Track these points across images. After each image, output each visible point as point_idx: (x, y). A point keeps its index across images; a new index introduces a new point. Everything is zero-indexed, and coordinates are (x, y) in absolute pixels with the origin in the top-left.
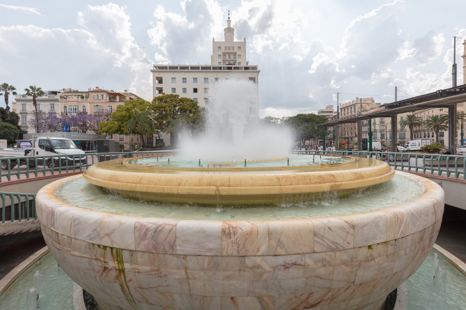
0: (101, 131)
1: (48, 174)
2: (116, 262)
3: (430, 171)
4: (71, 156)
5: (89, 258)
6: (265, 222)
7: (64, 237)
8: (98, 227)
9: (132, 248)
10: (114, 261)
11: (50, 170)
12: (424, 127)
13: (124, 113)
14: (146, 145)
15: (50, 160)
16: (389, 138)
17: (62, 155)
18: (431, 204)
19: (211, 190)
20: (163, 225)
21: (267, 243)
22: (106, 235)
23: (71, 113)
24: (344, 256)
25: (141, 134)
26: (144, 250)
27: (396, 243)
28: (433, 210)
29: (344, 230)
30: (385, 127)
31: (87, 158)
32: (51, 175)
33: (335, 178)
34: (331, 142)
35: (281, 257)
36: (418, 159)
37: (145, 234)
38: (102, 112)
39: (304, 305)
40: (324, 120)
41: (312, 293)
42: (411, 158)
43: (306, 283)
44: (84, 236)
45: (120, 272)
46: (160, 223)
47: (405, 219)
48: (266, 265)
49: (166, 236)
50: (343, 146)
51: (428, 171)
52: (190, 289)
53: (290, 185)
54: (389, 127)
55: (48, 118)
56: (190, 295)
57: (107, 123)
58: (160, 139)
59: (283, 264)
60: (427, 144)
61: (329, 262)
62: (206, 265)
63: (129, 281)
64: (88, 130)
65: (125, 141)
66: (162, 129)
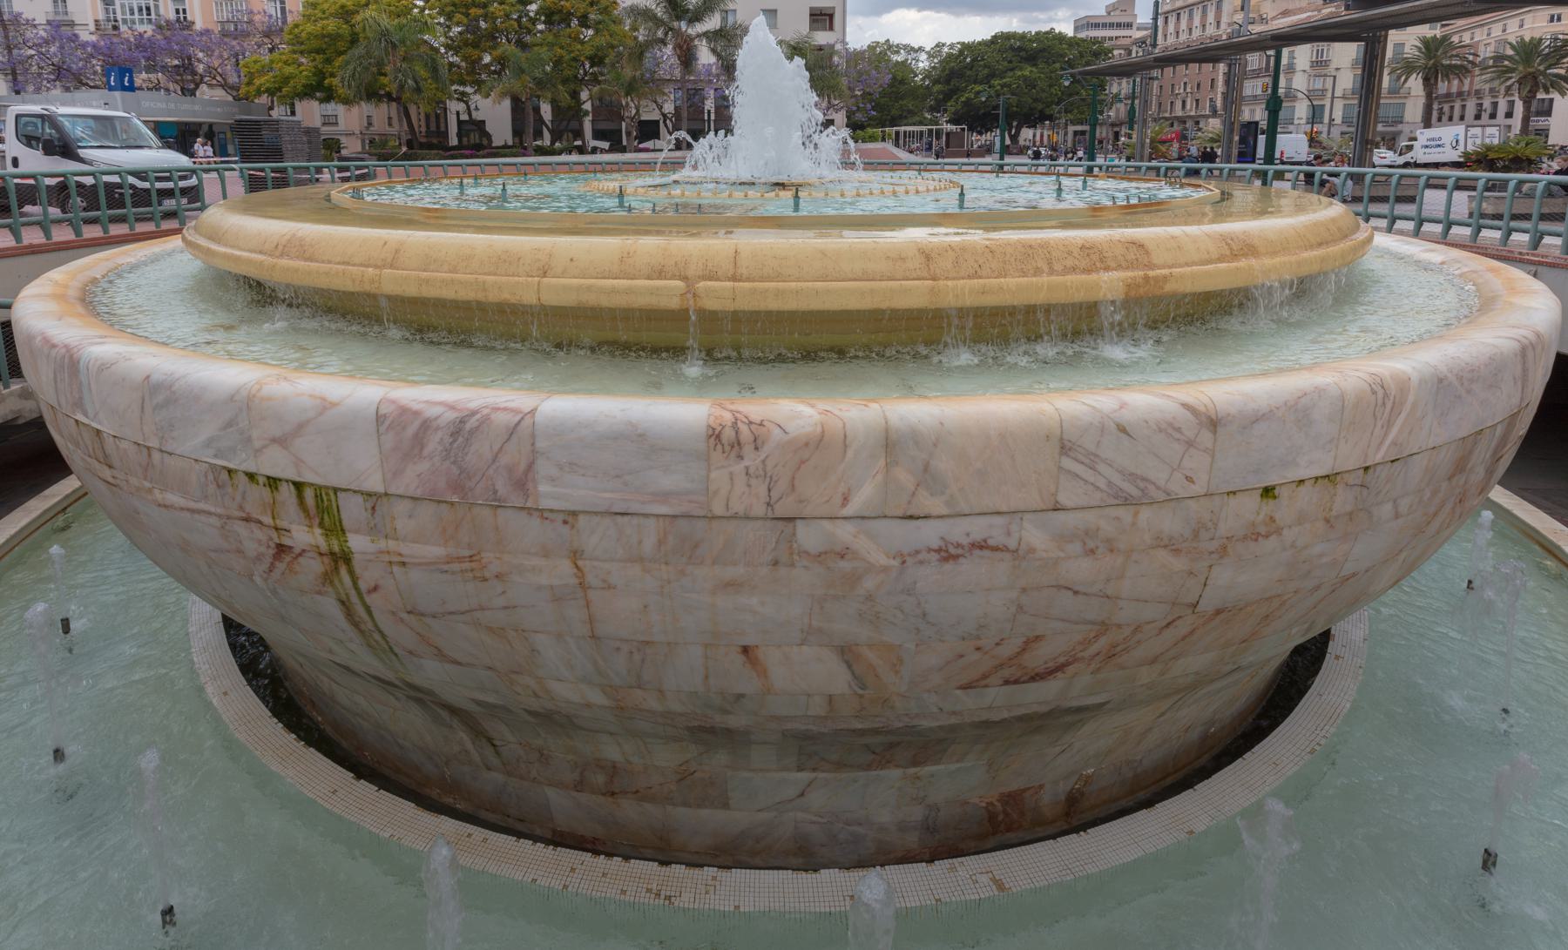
0: (252, 89)
1: (63, 234)
2: (318, 531)
3: (1497, 234)
4: (140, 174)
5: (219, 516)
6: (875, 406)
7: (124, 445)
8: (242, 411)
9: (375, 484)
10: (310, 527)
11: (70, 222)
12: (1479, 81)
13: (332, 25)
14: (423, 140)
15: (63, 187)
16: (1338, 120)
17: (105, 168)
18: (1516, 345)
19: (668, 293)
20: (486, 411)
21: (880, 477)
22: (274, 440)
23: (133, 22)
24: (1169, 523)
25: (398, 100)
26: (418, 493)
27: (1373, 485)
28: (1519, 367)
29: (1178, 436)
30: (1330, 81)
31: (200, 180)
32: (73, 237)
33: (1147, 253)
34: (1117, 135)
35: (931, 522)
36: (1456, 194)
37: (419, 440)
38: (250, 22)
39: (1006, 673)
40: (1096, 55)
41: (1038, 638)
42: (1428, 192)
43: (1020, 607)
44: (193, 443)
45: (336, 562)
46: (473, 405)
47: (1411, 398)
48: (874, 548)
49: (496, 448)
50: (1163, 149)
51: (1491, 235)
52: (591, 620)
53: (969, 277)
54: (1347, 80)
55: (47, 42)
56: (593, 637)
57: (272, 62)
58: (472, 121)
59: (936, 544)
60: (1487, 141)
61: (1108, 541)
62: (649, 544)
63: (369, 592)
64: (204, 87)
65: (342, 126)
66: (478, 84)
